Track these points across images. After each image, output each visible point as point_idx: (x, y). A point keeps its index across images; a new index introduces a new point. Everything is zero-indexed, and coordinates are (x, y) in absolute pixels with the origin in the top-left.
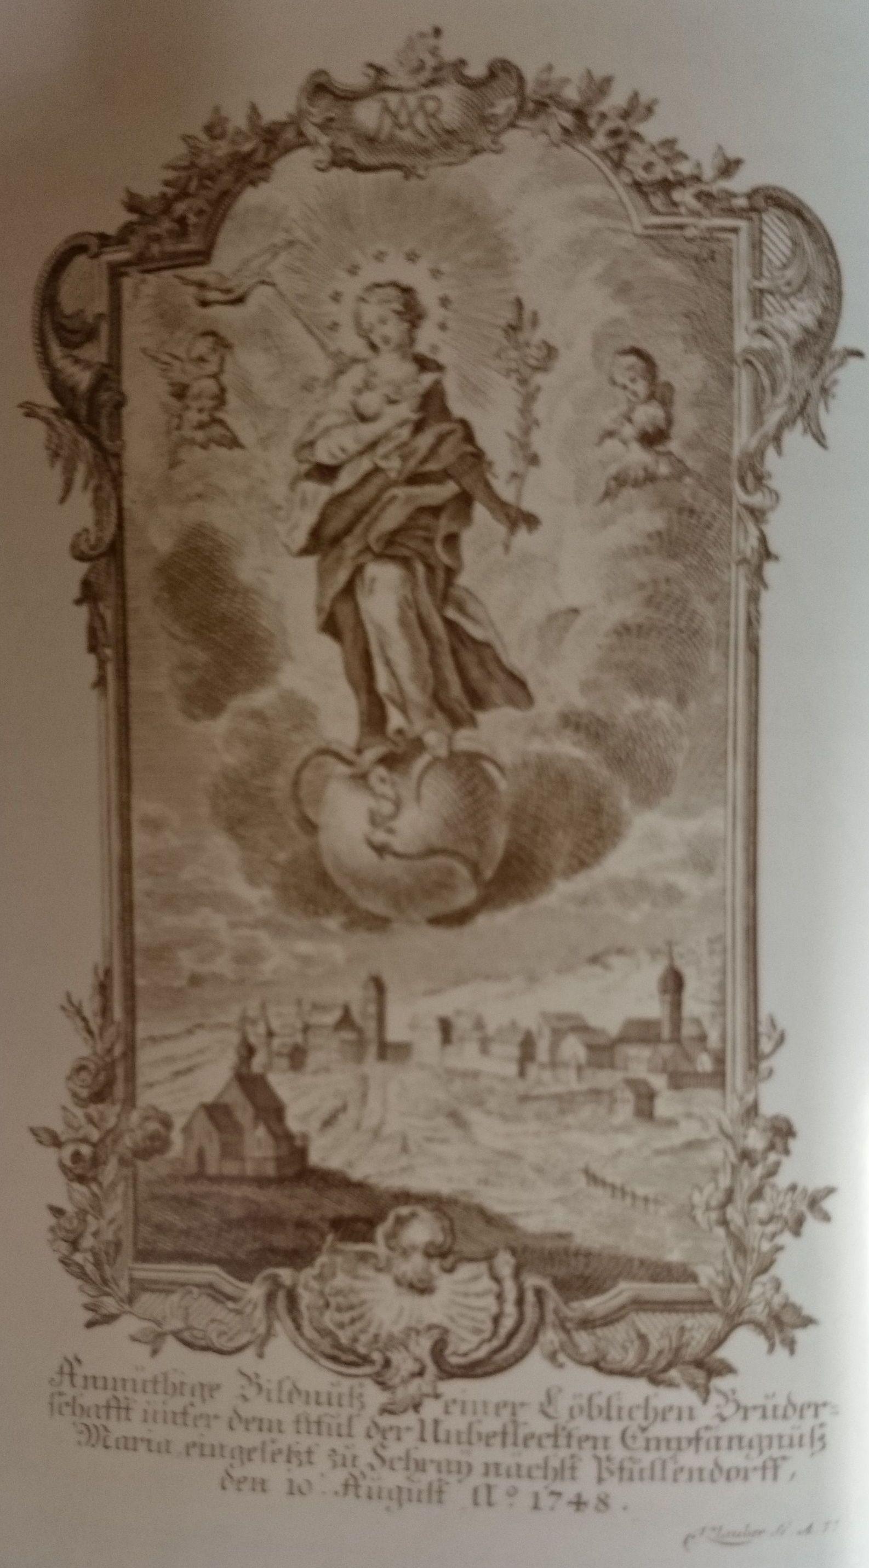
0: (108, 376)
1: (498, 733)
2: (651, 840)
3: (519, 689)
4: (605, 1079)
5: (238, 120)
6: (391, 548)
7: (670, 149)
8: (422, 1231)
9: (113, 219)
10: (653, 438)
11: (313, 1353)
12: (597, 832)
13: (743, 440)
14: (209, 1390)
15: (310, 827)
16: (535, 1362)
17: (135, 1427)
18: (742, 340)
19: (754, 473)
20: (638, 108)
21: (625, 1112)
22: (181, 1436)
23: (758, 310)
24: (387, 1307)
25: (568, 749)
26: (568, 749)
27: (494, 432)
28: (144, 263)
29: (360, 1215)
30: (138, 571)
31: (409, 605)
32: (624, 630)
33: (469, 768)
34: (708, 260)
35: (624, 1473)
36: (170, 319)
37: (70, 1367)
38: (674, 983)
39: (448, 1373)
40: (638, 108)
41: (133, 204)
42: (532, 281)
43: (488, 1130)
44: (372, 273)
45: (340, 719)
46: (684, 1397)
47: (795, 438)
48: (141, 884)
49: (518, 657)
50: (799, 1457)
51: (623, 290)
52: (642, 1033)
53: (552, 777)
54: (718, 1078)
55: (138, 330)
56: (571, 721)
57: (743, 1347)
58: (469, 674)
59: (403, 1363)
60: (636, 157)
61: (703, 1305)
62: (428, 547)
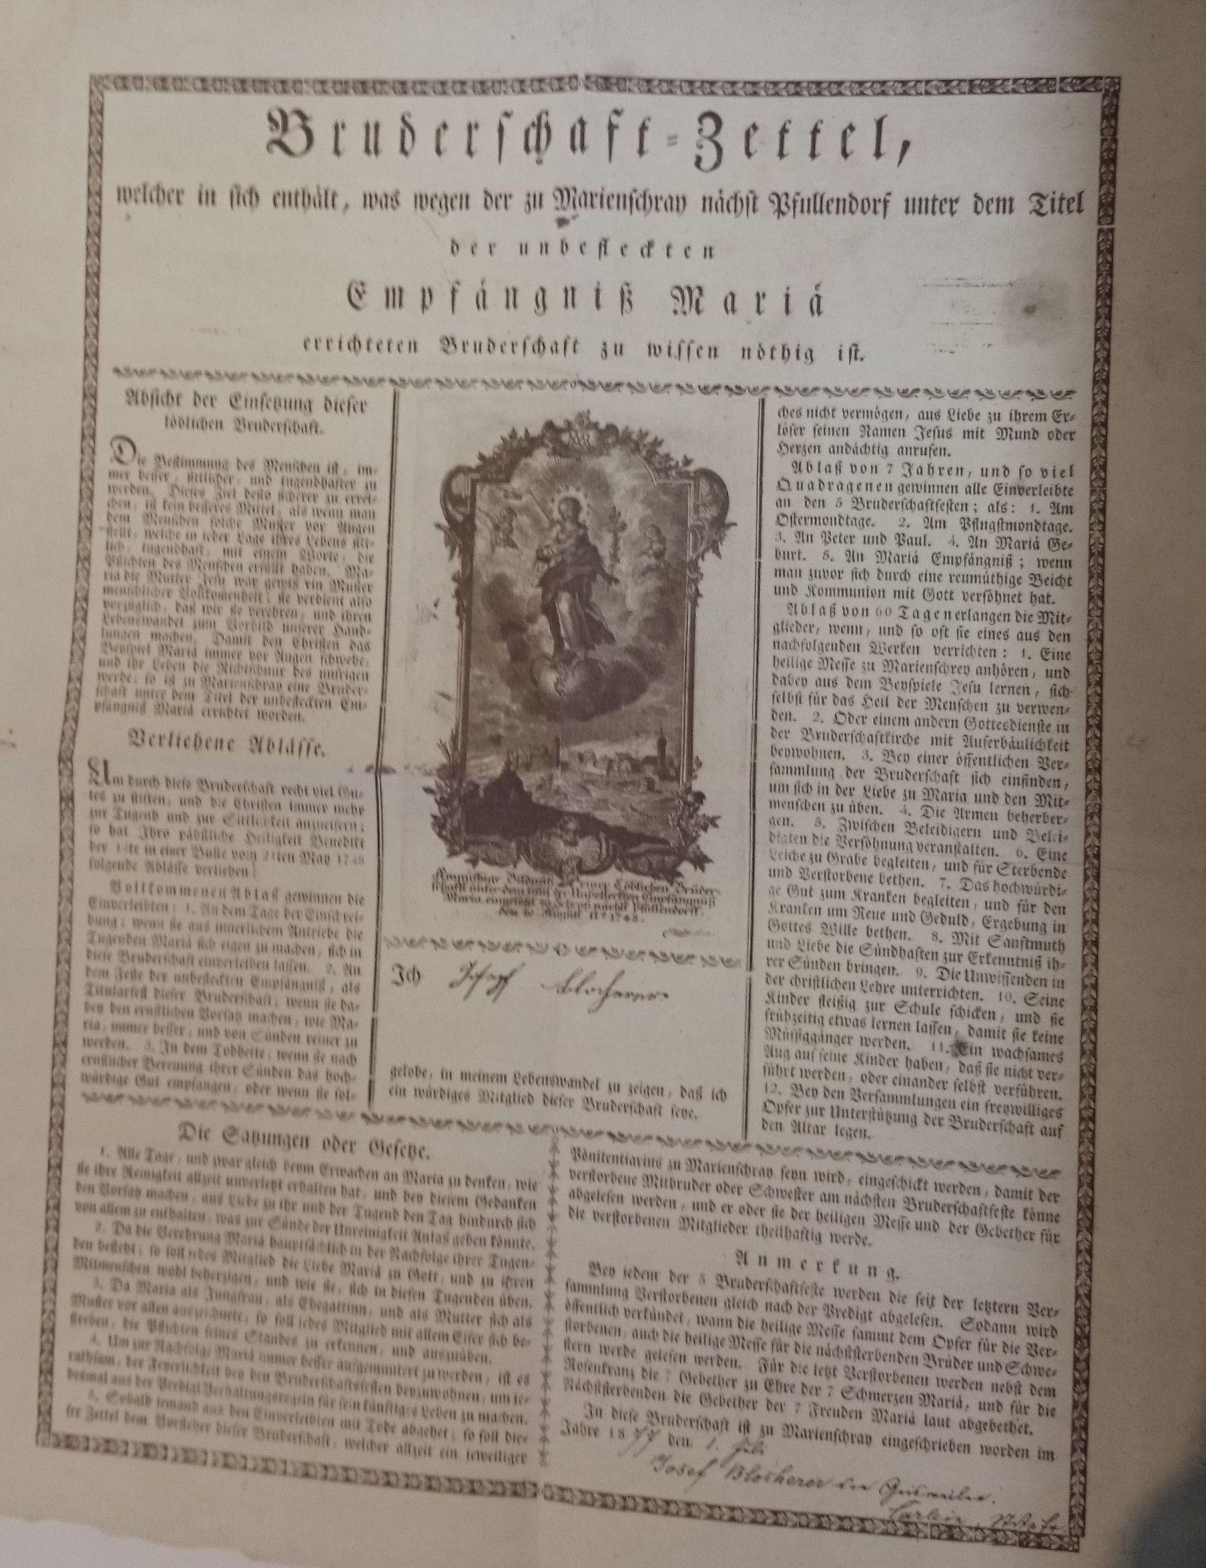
0: (470, 518)
1: (602, 653)
2: (653, 697)
3: (610, 638)
4: (636, 777)
5: (521, 434)
6: (568, 587)
7: (668, 457)
8: (572, 826)
9: (474, 462)
10: (659, 555)
11: (536, 866)
12: (638, 689)
13: (691, 554)
14: (494, 879)
15: (536, 683)
16: (613, 870)
17: (467, 893)
18: (691, 522)
19: (694, 566)
20: (657, 443)
21: (643, 788)
22: (484, 896)
23: (697, 511)
24: (562, 850)
25: (629, 660)
26: (629, 660)
27: (605, 550)
28: (485, 480)
29: (551, 818)
30: (477, 590)
31: (572, 607)
32: (647, 620)
33: (590, 665)
34: (680, 495)
35: (643, 908)
36: (493, 499)
37: (441, 872)
38: (662, 744)
39: (582, 872)
40: (657, 443)
41: (481, 457)
42: (618, 500)
43: (595, 793)
44: (564, 494)
45: (548, 647)
46: (664, 883)
47: (710, 556)
48: (473, 701)
49: (613, 628)
50: (705, 908)
51: (650, 505)
52: (649, 760)
53: (620, 669)
54: (677, 778)
55: (482, 503)
56: (629, 650)
57: (686, 868)
58: (593, 631)
59: (567, 869)
60: (656, 459)
61: (669, 852)
62: (581, 592)
